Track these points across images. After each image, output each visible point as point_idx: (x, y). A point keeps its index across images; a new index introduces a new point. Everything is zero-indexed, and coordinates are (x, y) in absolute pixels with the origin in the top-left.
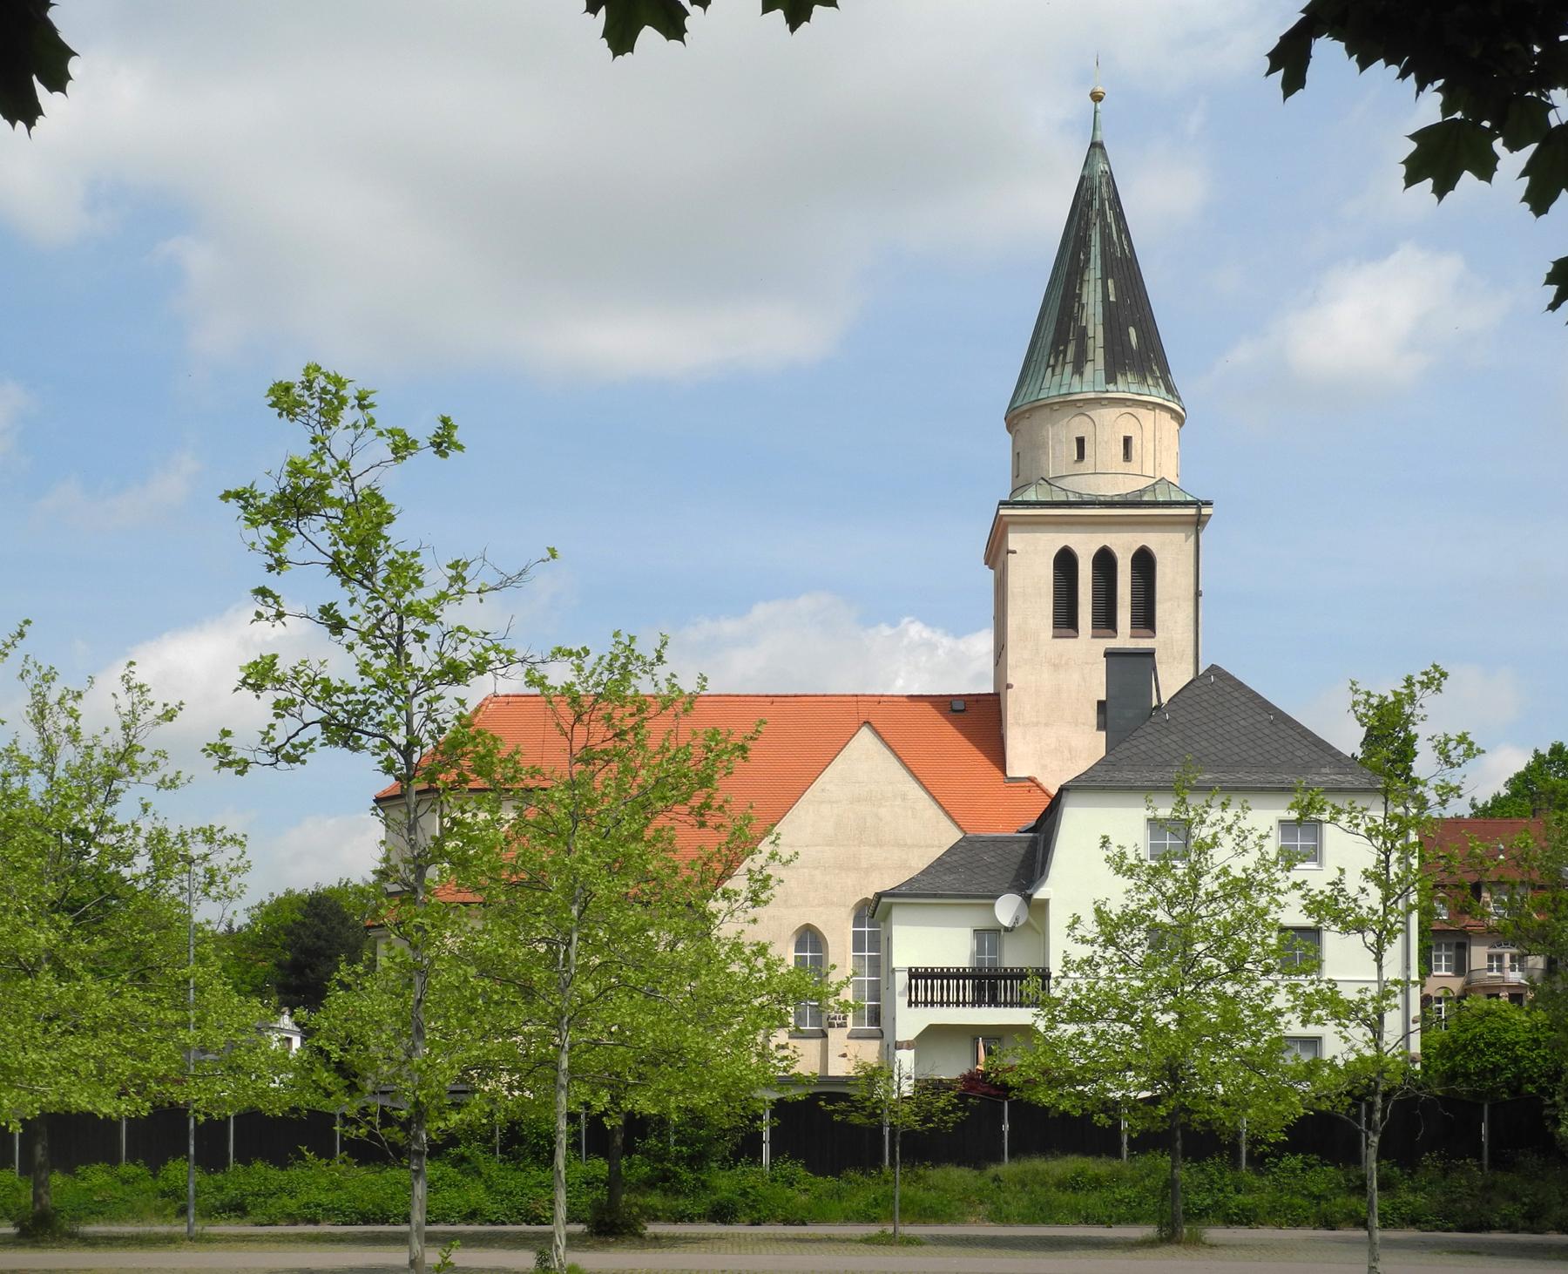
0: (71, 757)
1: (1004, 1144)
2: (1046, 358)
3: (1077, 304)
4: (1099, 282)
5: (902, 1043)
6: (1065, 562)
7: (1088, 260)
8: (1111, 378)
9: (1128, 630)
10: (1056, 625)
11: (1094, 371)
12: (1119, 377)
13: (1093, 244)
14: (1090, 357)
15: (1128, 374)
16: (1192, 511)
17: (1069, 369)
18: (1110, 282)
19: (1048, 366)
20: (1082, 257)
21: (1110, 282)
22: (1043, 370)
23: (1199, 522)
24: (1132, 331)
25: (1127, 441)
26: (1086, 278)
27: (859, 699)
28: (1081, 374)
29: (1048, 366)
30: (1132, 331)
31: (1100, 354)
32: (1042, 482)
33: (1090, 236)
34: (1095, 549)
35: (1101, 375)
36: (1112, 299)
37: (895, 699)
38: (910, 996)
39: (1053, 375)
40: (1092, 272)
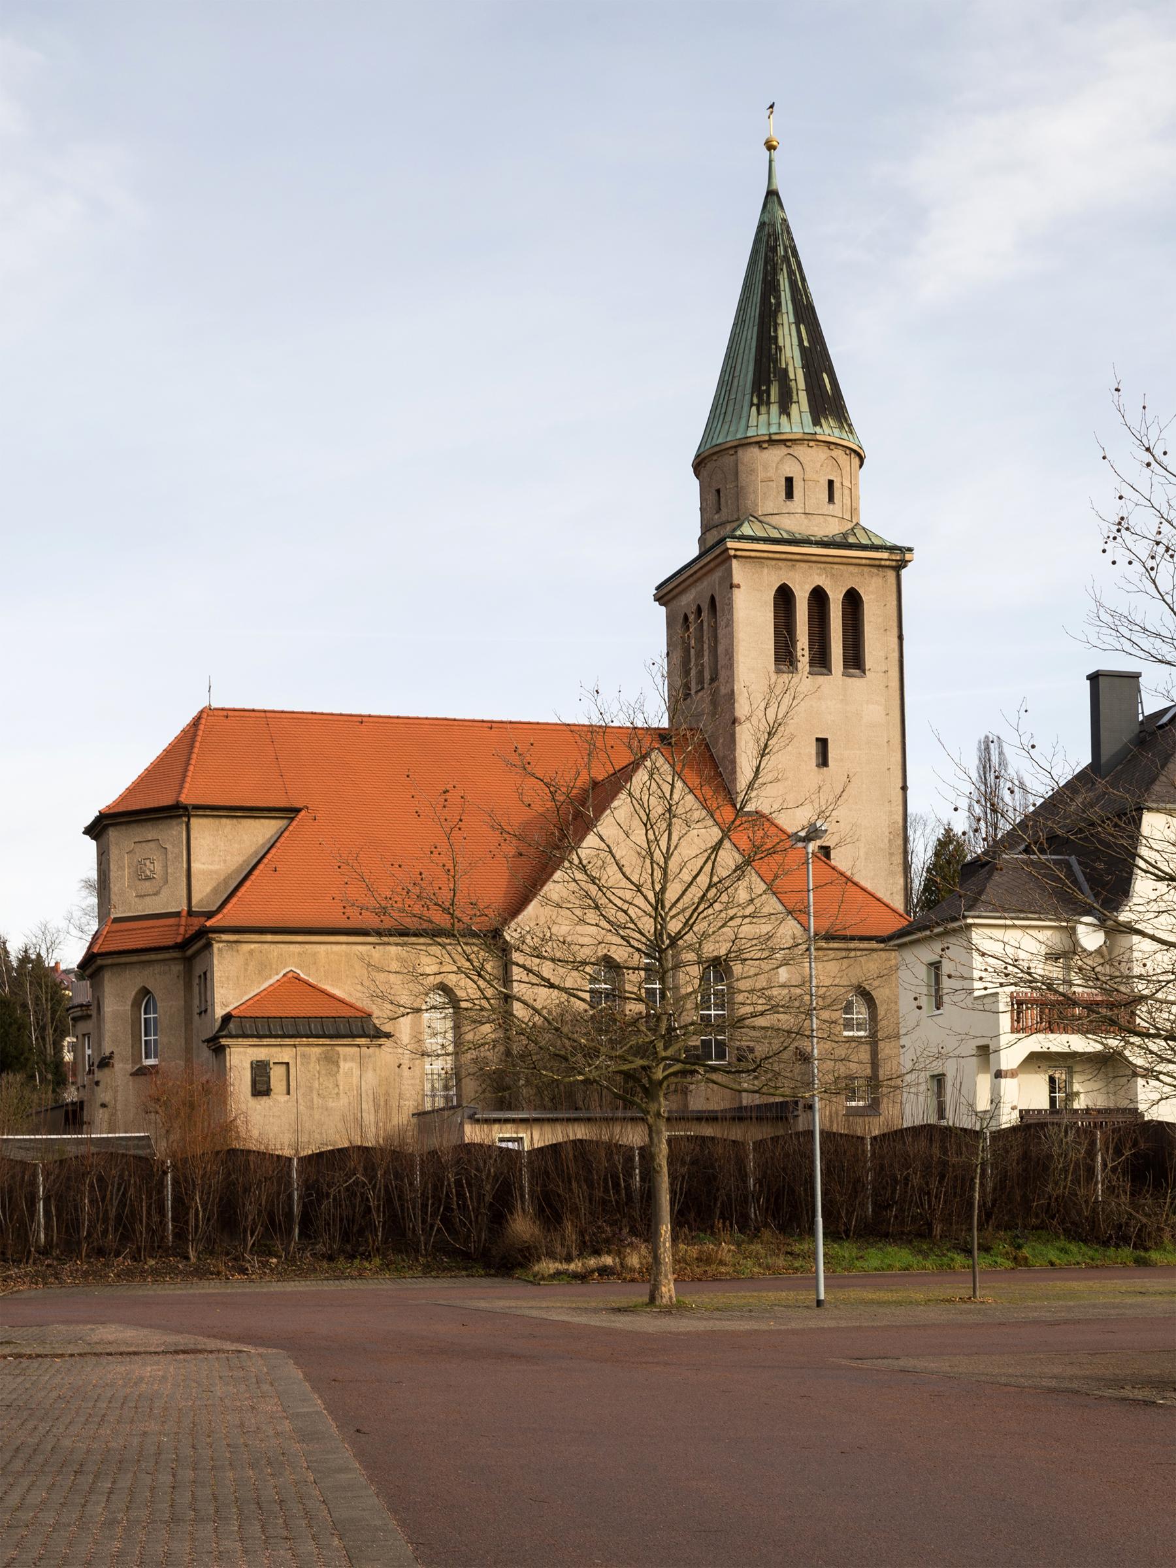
2: (748, 397)
3: (773, 346)
4: (793, 327)
5: (1006, 1071)
6: (784, 597)
7: (779, 304)
8: (816, 422)
9: (807, 668)
10: (778, 659)
11: (800, 412)
12: (822, 421)
13: (782, 288)
14: (795, 398)
17: (774, 409)
18: (802, 327)
19: (752, 405)
20: (773, 301)
21: (802, 327)
22: (746, 408)
23: (903, 564)
24: (825, 376)
25: (789, 481)
26: (779, 321)
27: (268, 715)
28: (788, 415)
29: (752, 405)
30: (825, 376)
31: (803, 397)
32: (751, 518)
33: (779, 281)
34: (809, 588)
35: (807, 418)
36: (806, 344)
37: (411, 721)
39: (759, 413)
40: (785, 316)
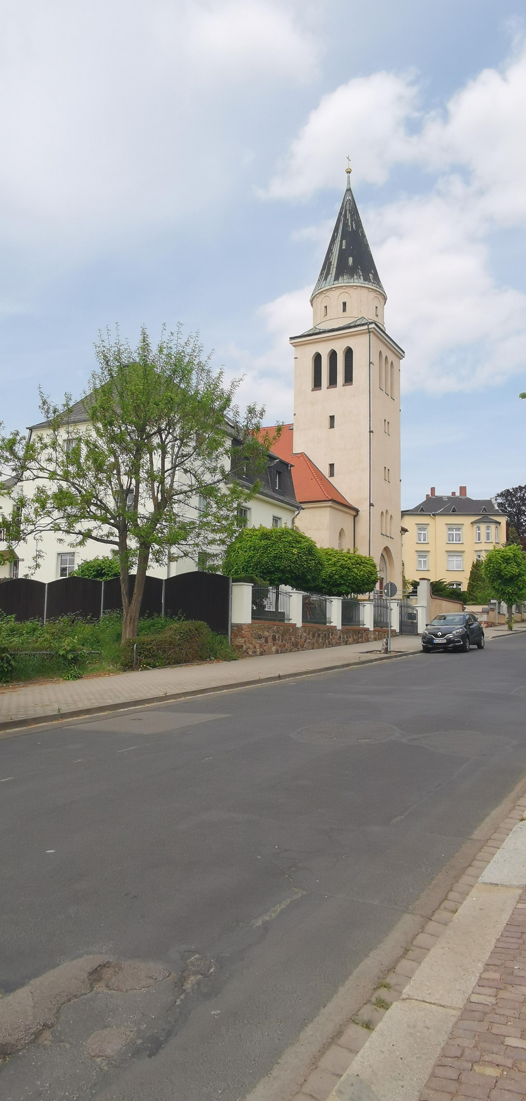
0: (8, 468)
1: (104, 586)
6: (318, 358)
14: (331, 273)
15: (345, 276)
16: (366, 327)
34: (328, 351)
36: (344, 247)
38: (390, 529)
